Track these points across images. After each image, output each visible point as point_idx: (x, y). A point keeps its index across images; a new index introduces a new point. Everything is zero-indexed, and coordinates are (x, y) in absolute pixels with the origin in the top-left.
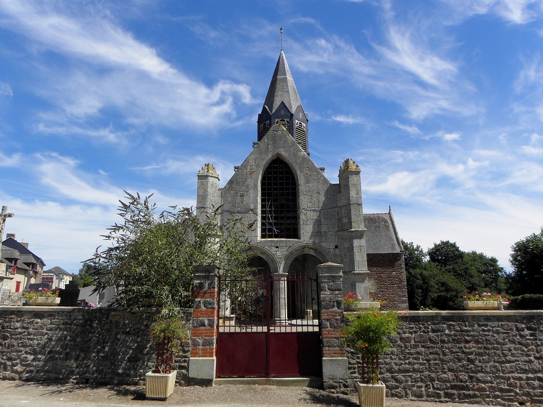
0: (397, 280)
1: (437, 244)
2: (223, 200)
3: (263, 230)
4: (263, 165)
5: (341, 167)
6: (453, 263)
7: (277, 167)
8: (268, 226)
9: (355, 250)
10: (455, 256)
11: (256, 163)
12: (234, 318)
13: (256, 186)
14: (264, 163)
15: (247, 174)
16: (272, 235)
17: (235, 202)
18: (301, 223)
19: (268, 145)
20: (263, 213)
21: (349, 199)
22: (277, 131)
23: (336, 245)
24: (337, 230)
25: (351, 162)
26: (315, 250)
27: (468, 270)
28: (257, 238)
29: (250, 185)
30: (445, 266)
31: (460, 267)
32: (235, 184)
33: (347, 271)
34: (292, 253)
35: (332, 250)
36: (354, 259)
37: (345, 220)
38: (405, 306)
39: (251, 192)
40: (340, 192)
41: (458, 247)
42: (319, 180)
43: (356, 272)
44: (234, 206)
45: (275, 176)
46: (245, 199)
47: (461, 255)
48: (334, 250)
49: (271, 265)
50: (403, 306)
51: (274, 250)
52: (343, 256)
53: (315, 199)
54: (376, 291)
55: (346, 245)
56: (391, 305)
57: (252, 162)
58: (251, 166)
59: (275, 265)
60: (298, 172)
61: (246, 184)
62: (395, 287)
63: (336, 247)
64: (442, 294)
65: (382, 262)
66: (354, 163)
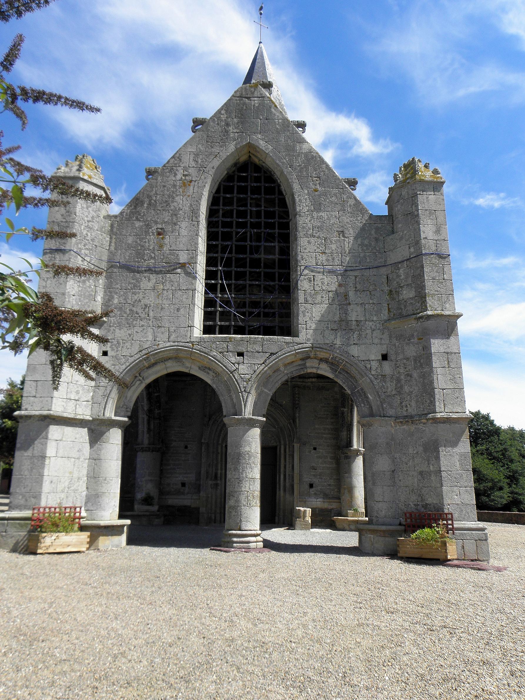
2: (114, 240)
3: (208, 316)
4: (213, 168)
5: (395, 175)
6: (487, 441)
7: (246, 177)
8: (221, 306)
9: (436, 362)
10: (489, 431)
11: (197, 162)
12: (125, 528)
13: (195, 213)
14: (216, 163)
15: (174, 186)
16: (229, 327)
17: (142, 246)
18: (301, 299)
19: (228, 125)
20: (210, 275)
21: (417, 242)
22: (248, 98)
23: (385, 352)
24: (385, 318)
25: (421, 166)
26: (333, 364)
27: (506, 452)
28: (192, 332)
29: (180, 209)
31: (495, 447)
32: (145, 205)
33: (413, 413)
34: (278, 370)
35: (374, 364)
36: (432, 382)
37: (407, 294)
39: (184, 225)
40: (393, 232)
41: (493, 420)
42: (343, 206)
43: (439, 415)
44: (140, 255)
45: (242, 196)
46: (167, 241)
47: (497, 431)
48: (381, 364)
49: (224, 399)
51: (233, 360)
52: (402, 377)
53: (334, 247)
55: (411, 351)
57: (188, 160)
58: (185, 169)
59: (234, 396)
60: (296, 187)
61: (172, 207)
63: (385, 357)
66: (426, 166)
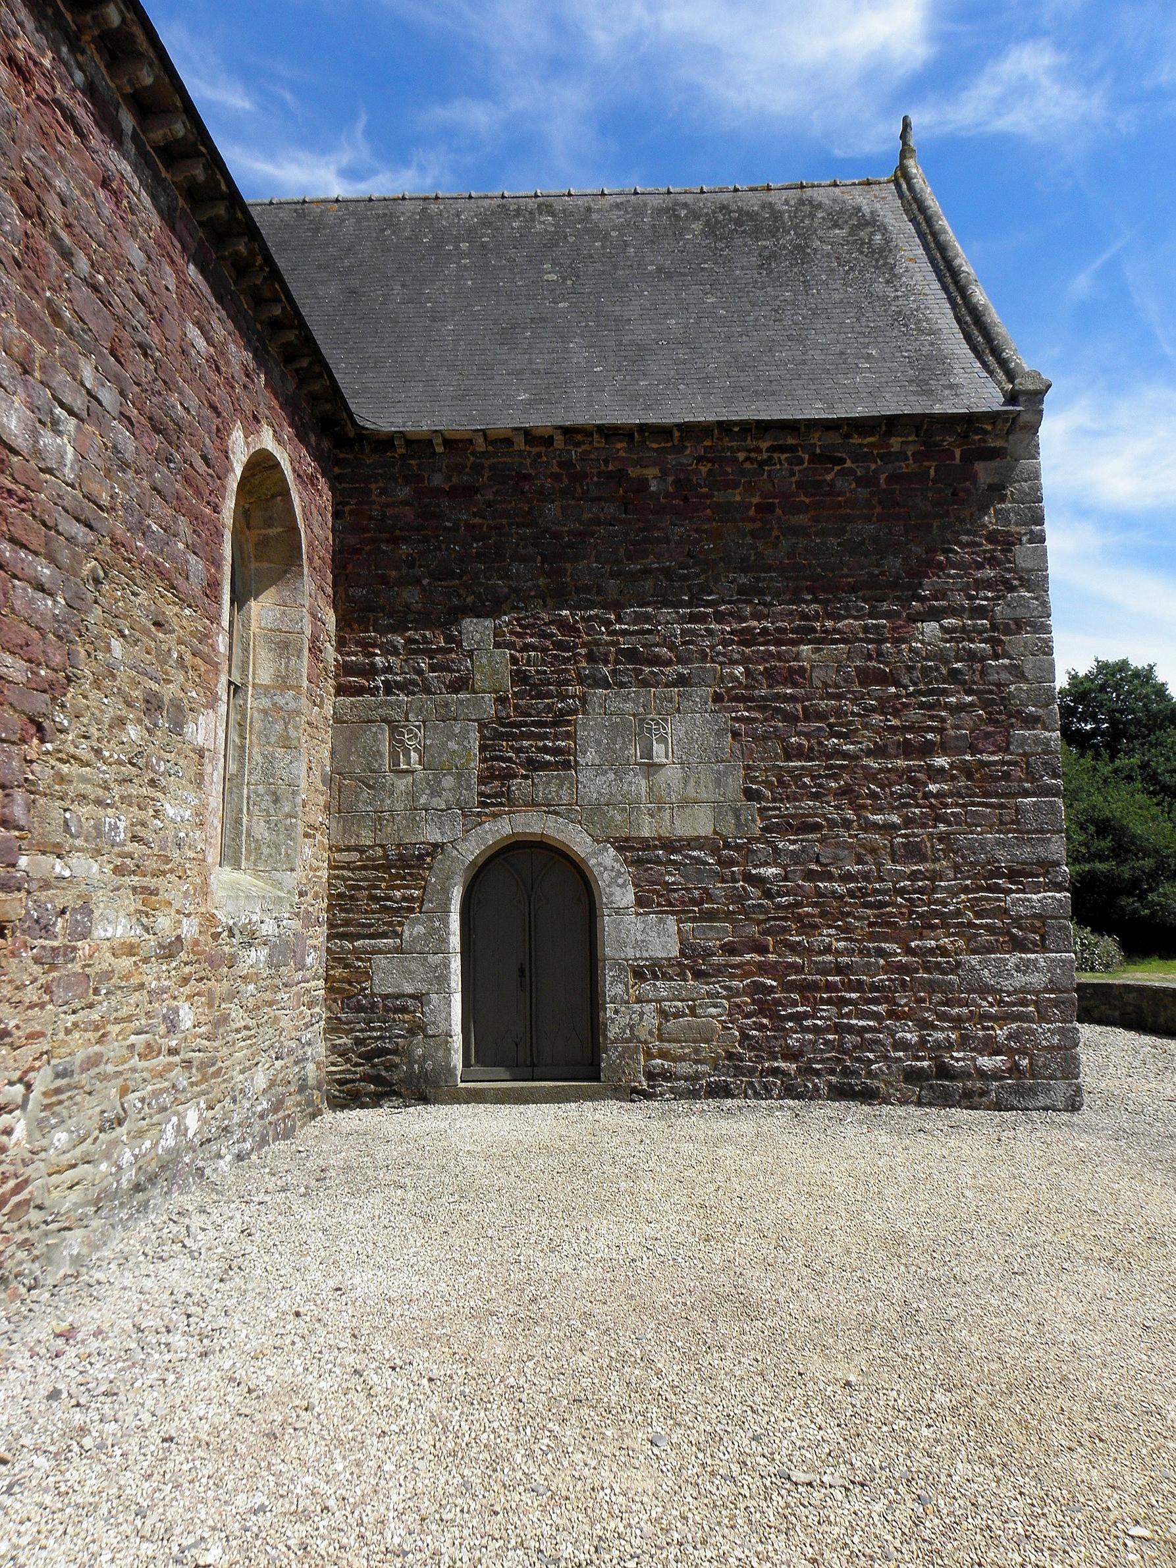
0: (961, 708)
1: (1081, 674)
6: (1143, 745)
30: (1112, 760)
38: (1037, 980)
50: (1020, 980)
54: (729, 827)
56: (889, 968)
62: (936, 774)
64: (1099, 866)
65: (802, 519)
